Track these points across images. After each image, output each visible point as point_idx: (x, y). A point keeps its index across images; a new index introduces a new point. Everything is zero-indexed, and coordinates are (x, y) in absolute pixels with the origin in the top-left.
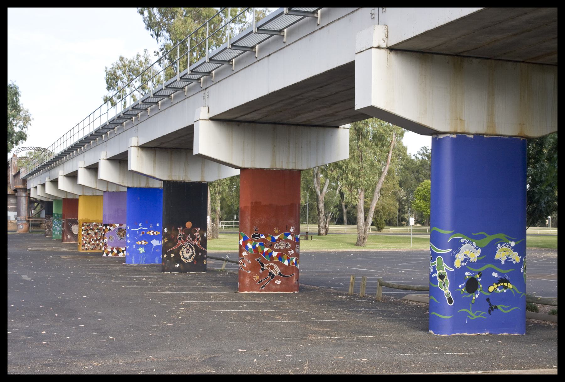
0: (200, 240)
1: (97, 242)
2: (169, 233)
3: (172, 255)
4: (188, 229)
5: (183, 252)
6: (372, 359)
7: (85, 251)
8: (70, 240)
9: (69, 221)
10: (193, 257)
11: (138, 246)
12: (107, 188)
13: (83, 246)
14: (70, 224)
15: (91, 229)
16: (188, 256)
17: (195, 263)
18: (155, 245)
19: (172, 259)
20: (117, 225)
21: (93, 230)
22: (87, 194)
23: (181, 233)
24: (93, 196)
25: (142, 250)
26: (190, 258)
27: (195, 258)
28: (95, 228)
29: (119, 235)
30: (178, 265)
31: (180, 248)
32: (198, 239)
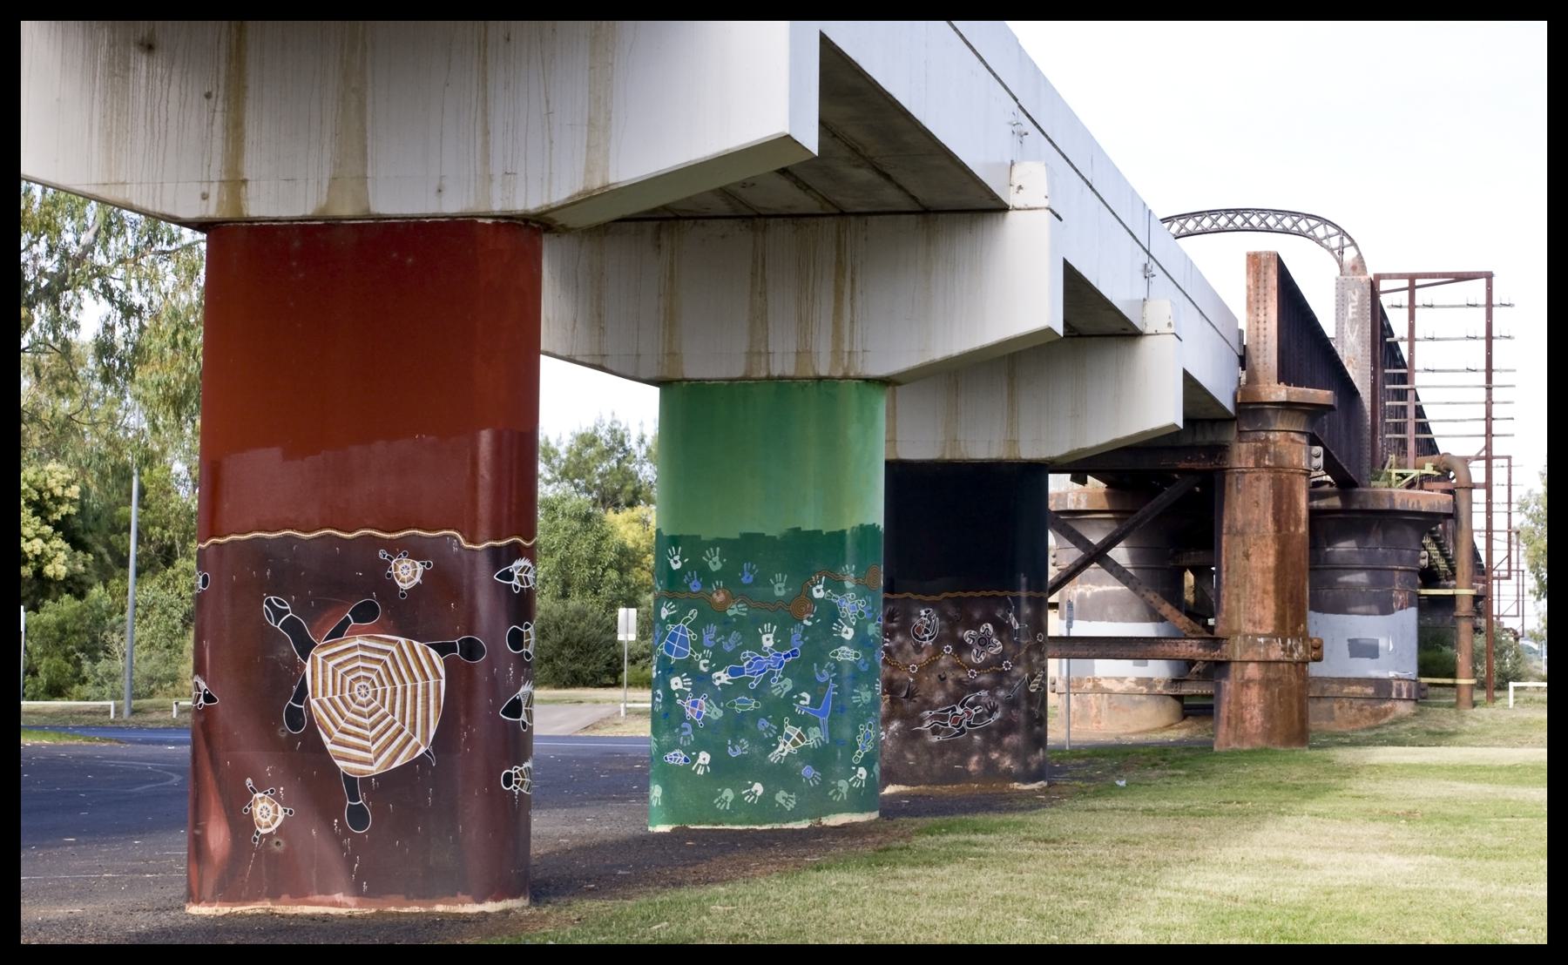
14: (277, 610)
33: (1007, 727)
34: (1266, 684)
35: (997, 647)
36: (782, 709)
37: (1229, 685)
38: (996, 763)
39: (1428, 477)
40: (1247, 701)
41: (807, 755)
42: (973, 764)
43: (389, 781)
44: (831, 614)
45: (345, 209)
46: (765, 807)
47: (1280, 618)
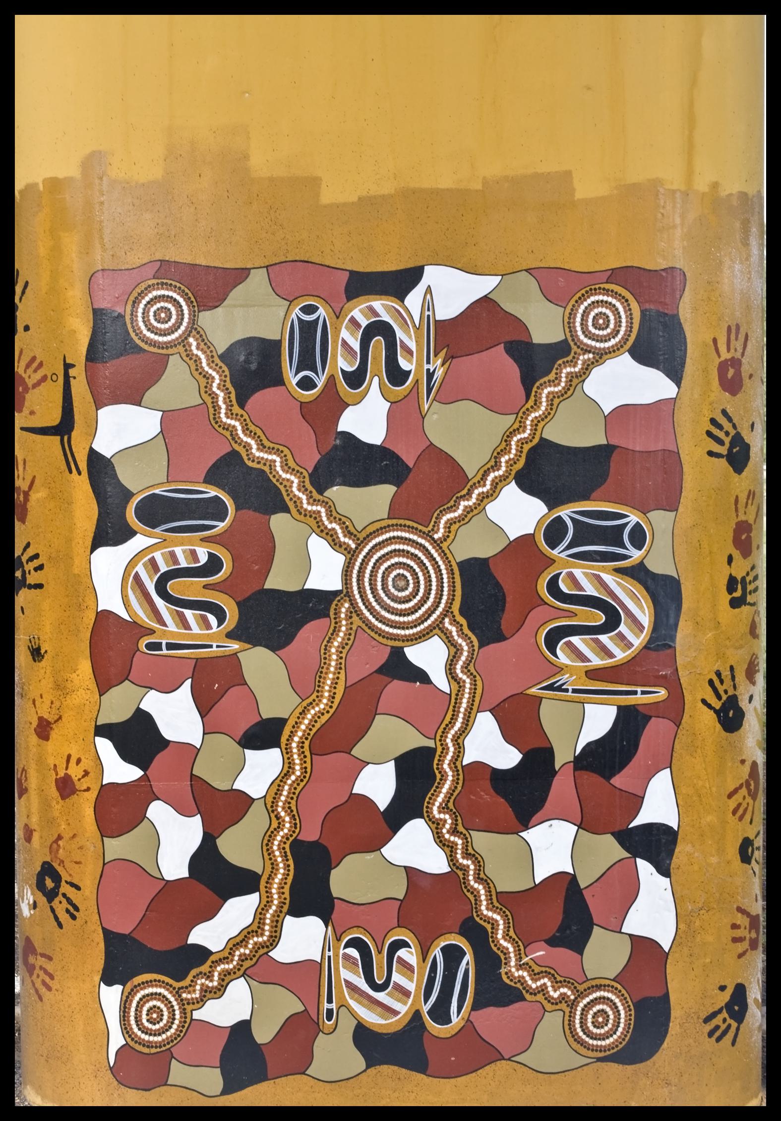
6: (664, 207)
15: (353, 463)
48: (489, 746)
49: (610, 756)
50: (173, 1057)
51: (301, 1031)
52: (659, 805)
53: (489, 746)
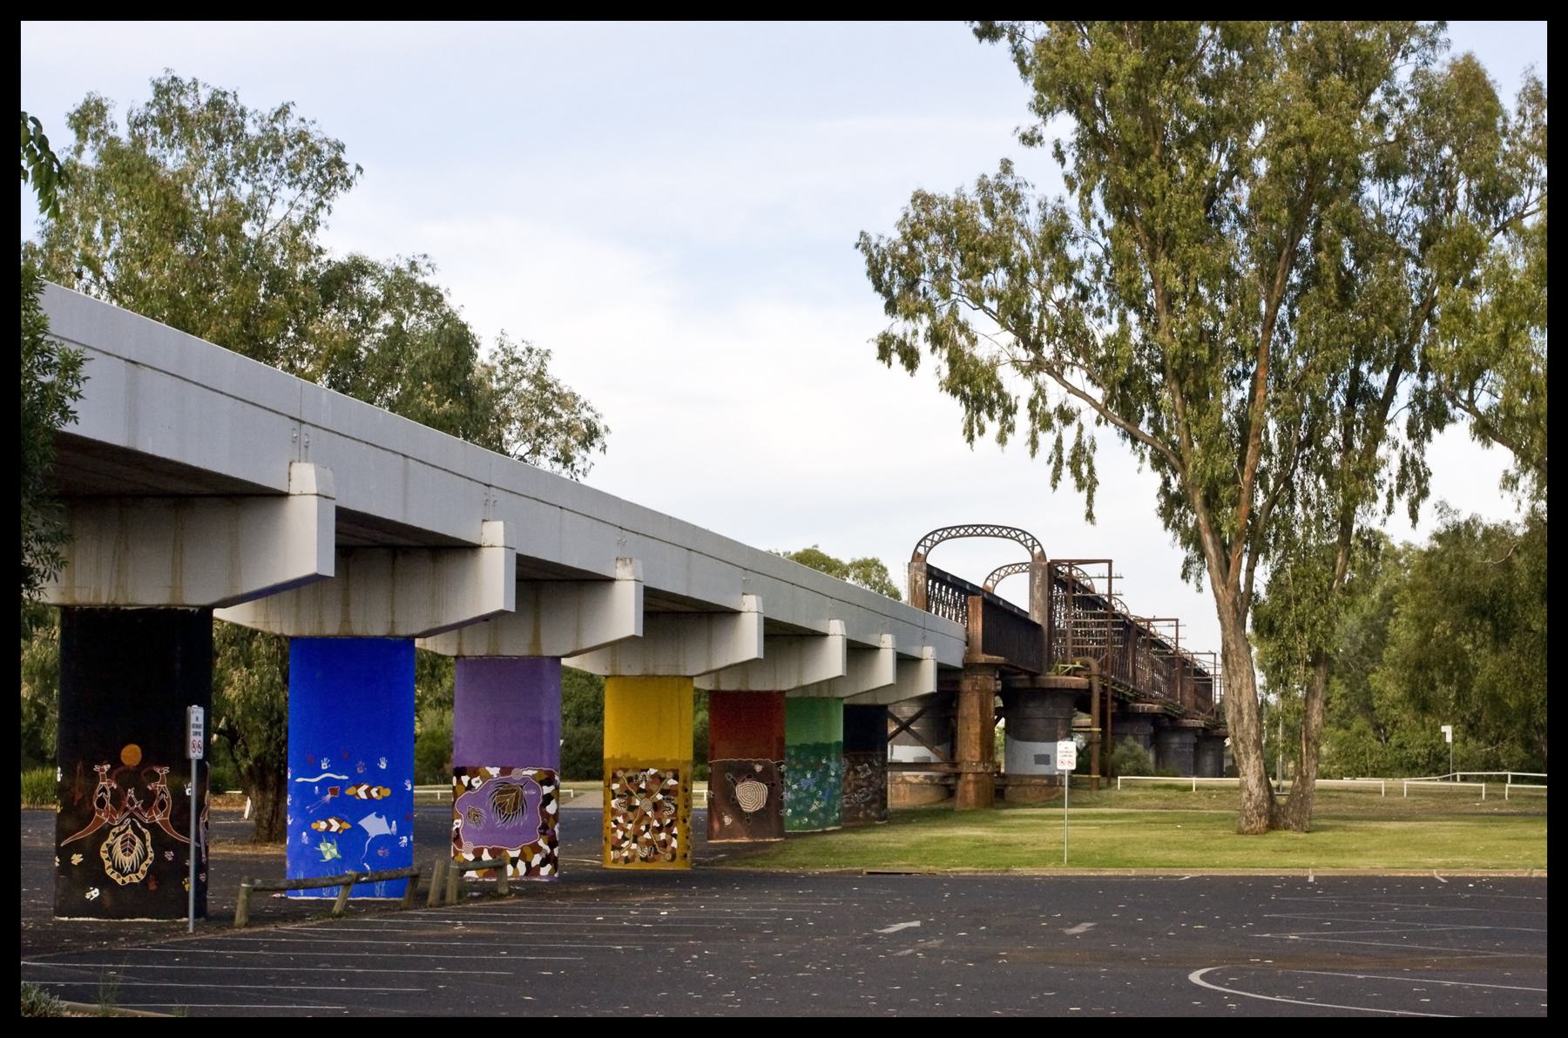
0: (169, 806)
1: (663, 836)
2: (67, 784)
3: (77, 859)
4: (127, 771)
5: (111, 848)
7: (621, 866)
8: (729, 832)
9: (729, 767)
10: (144, 867)
11: (317, 837)
12: (460, 644)
13: (617, 847)
14: (729, 776)
15: (640, 791)
16: (127, 861)
17: (152, 887)
18: (373, 833)
19: (76, 872)
20: (494, 771)
21: (648, 793)
22: (624, 673)
23: (107, 784)
24: (647, 676)
25: (329, 851)
26: (135, 870)
27: (150, 868)
28: (654, 787)
29: (501, 807)
30: (94, 893)
31: (103, 834)
32: (162, 805)
33: (873, 801)
34: (976, 782)
35: (870, 772)
36: (813, 796)
37: (961, 783)
38: (873, 810)
39: (1077, 669)
40: (968, 789)
41: (820, 810)
42: (861, 815)
43: (756, 813)
44: (827, 768)
45: (743, 689)
46: (809, 825)
47: (982, 754)
48: (656, 824)
49: (670, 825)
50: (558, 659)
51: (634, 857)
52: (675, 831)
53: (656, 824)
